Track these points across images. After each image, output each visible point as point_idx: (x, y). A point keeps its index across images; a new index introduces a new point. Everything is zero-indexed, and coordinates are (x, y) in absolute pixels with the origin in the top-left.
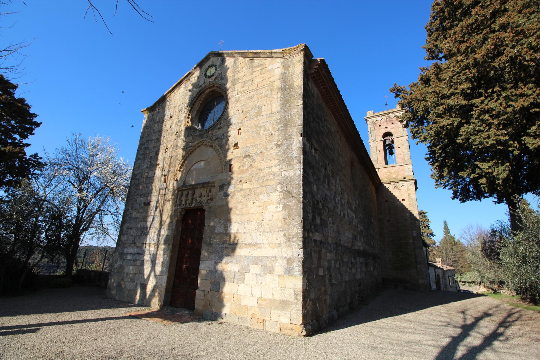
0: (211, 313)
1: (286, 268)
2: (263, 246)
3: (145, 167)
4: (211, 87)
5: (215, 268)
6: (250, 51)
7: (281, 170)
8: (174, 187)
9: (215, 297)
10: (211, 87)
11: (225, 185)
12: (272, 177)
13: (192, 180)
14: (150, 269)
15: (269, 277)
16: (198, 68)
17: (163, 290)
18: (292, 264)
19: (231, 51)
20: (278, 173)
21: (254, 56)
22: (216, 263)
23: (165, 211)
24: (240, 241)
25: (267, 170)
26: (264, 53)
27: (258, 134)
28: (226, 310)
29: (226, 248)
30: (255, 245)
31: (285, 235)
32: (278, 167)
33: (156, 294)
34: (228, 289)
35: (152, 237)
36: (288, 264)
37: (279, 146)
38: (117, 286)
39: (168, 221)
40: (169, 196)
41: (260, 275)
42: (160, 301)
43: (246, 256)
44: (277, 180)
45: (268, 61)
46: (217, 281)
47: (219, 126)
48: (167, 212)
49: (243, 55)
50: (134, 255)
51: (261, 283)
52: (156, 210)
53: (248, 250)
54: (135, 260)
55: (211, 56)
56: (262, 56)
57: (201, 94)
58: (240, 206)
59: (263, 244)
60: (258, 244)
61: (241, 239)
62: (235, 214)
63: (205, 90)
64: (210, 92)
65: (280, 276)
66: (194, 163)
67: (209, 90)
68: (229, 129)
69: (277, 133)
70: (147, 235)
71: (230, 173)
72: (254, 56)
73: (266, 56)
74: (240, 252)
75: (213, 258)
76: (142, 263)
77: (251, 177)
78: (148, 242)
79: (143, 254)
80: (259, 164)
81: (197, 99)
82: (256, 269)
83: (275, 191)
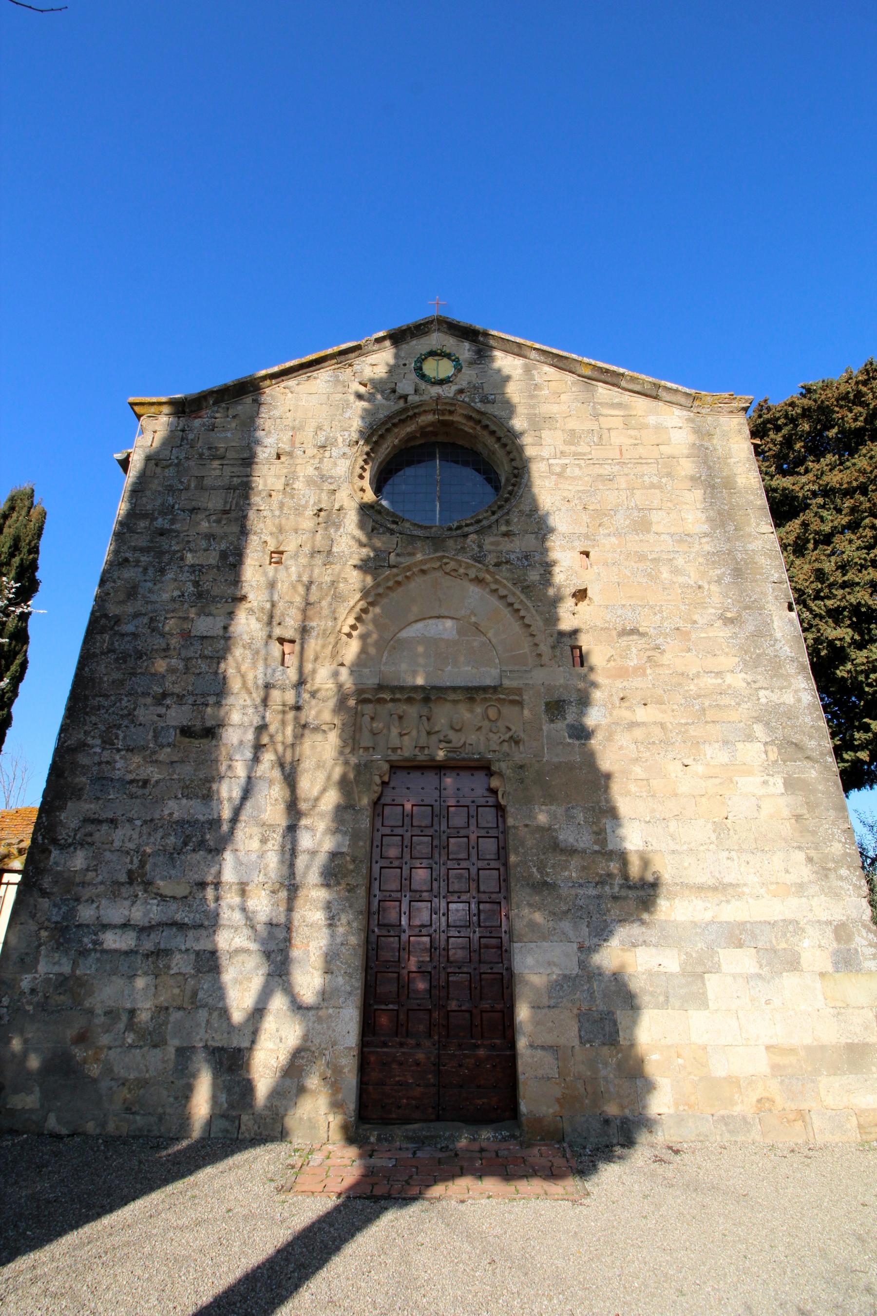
0: (587, 1128)
1: (836, 953)
2: (745, 889)
3: (166, 596)
4: (443, 412)
5: (583, 964)
6: (586, 360)
7: (754, 686)
8: (340, 686)
9: (606, 1064)
10: (443, 412)
11: (567, 706)
12: (726, 700)
13: (414, 673)
14: (257, 982)
15: (789, 980)
16: (387, 343)
17: (349, 1065)
18: (849, 939)
19: (518, 340)
20: (746, 692)
21: (596, 374)
22: (586, 950)
23: (307, 764)
24: (667, 876)
25: (710, 681)
26: (633, 379)
27: (653, 577)
28: (660, 1104)
29: (615, 898)
30: (720, 889)
31: (810, 860)
32: (743, 675)
33: (313, 1082)
34: (653, 1034)
35: (249, 863)
36: (838, 938)
37: (731, 621)
38: (47, 1069)
39: (331, 799)
40: (322, 712)
41: (759, 976)
42: (336, 1105)
43: (695, 924)
44: (746, 710)
45: (641, 403)
46: (602, 1007)
47: (504, 528)
48: (319, 765)
49: (560, 363)
50: (144, 930)
51: (768, 1002)
52: (256, 759)
53: (699, 904)
54: (160, 953)
55: (434, 326)
56: (623, 384)
57: (402, 421)
58: (638, 771)
59: (745, 885)
60: (731, 885)
61: (666, 869)
62: (628, 793)
63: (420, 414)
64: (432, 424)
65: (822, 975)
66: (413, 618)
67: (430, 418)
68: (548, 544)
69: (714, 588)
70: (217, 851)
71: (584, 670)
72: (596, 374)
73: (637, 388)
74: (670, 909)
75: (571, 934)
76: (209, 963)
77: (660, 692)
78: (229, 875)
79: (210, 923)
80: (673, 657)
81: (388, 430)
82: (739, 961)
83: (750, 738)
